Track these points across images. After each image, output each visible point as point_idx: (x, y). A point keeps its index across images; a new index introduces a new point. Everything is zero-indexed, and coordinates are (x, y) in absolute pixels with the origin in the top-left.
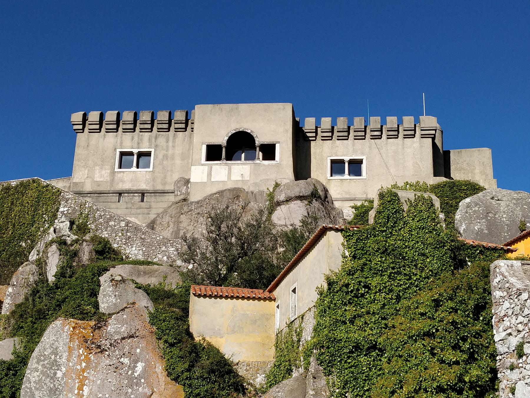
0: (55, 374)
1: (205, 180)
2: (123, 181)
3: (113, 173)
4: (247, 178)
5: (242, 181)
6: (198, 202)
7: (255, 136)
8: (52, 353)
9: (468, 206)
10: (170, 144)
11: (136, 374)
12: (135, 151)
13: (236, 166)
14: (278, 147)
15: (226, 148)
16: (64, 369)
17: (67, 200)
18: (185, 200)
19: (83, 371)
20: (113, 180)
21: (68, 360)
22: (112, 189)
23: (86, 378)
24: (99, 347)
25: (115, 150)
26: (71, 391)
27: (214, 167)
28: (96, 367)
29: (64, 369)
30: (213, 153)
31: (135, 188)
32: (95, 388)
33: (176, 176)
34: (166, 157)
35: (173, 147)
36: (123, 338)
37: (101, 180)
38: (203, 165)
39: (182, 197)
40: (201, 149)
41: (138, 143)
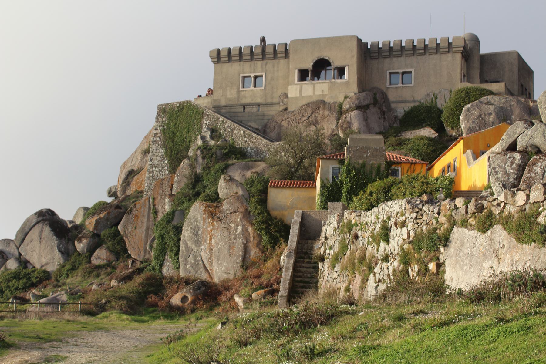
0: (197, 232)
1: (298, 95)
2: (245, 97)
3: (239, 91)
4: (326, 92)
5: (323, 95)
6: (293, 112)
7: (331, 61)
8: (195, 221)
9: (468, 110)
10: (276, 69)
11: (238, 233)
12: (253, 75)
13: (319, 85)
14: (347, 68)
15: (312, 71)
16: (201, 230)
17: (208, 115)
18: (286, 109)
19: (211, 231)
20: (239, 97)
21: (203, 225)
22: (239, 103)
23: (213, 235)
24: (219, 218)
25: (239, 75)
26: (205, 241)
27: (304, 86)
28: (218, 229)
29: (201, 230)
30: (303, 75)
31: (253, 102)
32: (217, 240)
33: (280, 92)
34: (272, 79)
35: (278, 71)
36: (231, 213)
37: (231, 96)
38: (296, 84)
39: (284, 107)
40: (295, 73)
41: (254, 69)
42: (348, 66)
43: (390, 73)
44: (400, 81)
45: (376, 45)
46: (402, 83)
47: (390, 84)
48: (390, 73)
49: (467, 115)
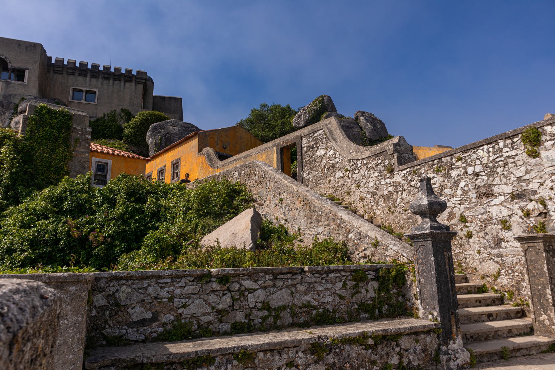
9: (155, 128)
42: (28, 69)
43: (74, 90)
44: (84, 98)
45: (60, 62)
46: (86, 100)
47: (73, 99)
48: (74, 90)
49: (154, 132)
